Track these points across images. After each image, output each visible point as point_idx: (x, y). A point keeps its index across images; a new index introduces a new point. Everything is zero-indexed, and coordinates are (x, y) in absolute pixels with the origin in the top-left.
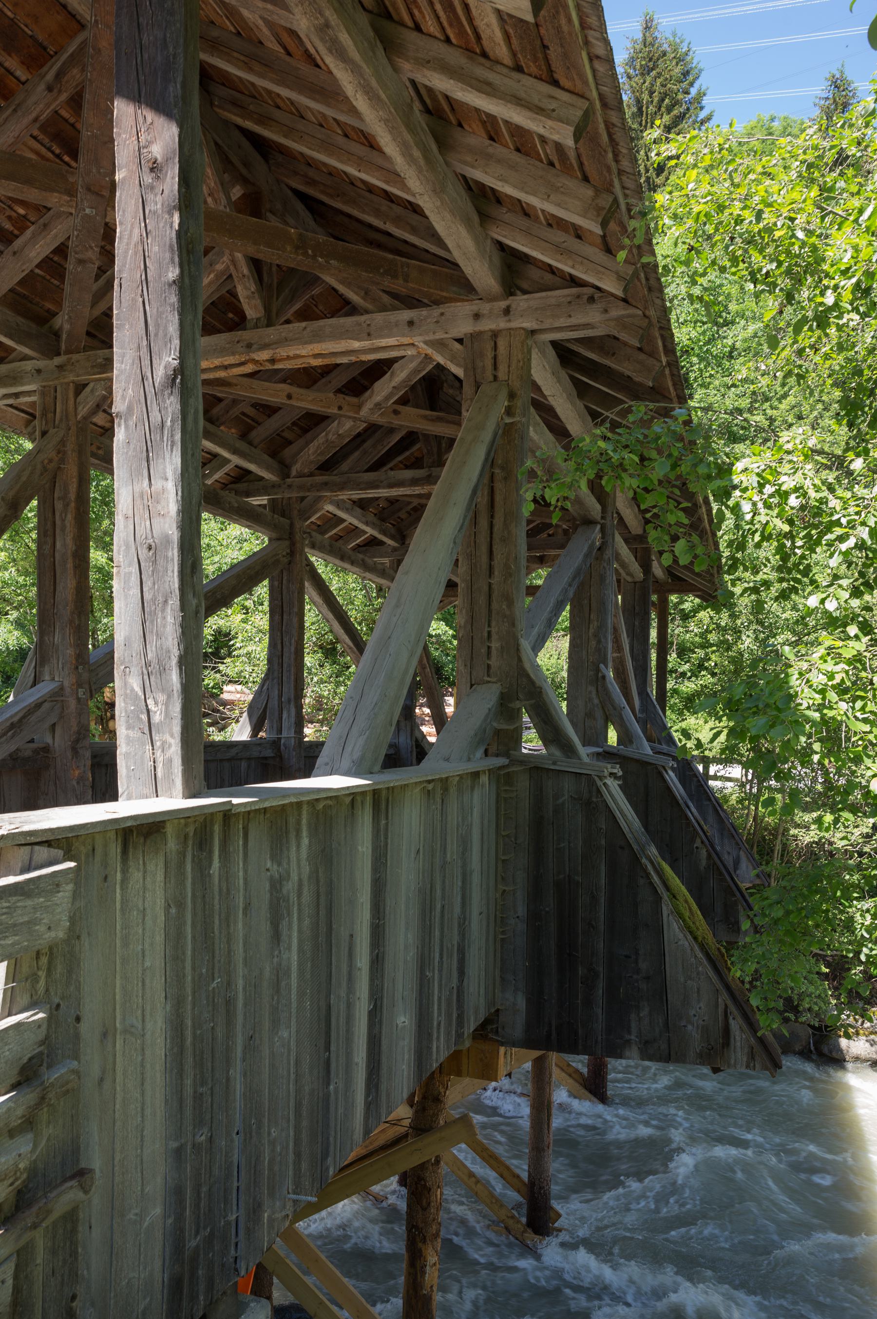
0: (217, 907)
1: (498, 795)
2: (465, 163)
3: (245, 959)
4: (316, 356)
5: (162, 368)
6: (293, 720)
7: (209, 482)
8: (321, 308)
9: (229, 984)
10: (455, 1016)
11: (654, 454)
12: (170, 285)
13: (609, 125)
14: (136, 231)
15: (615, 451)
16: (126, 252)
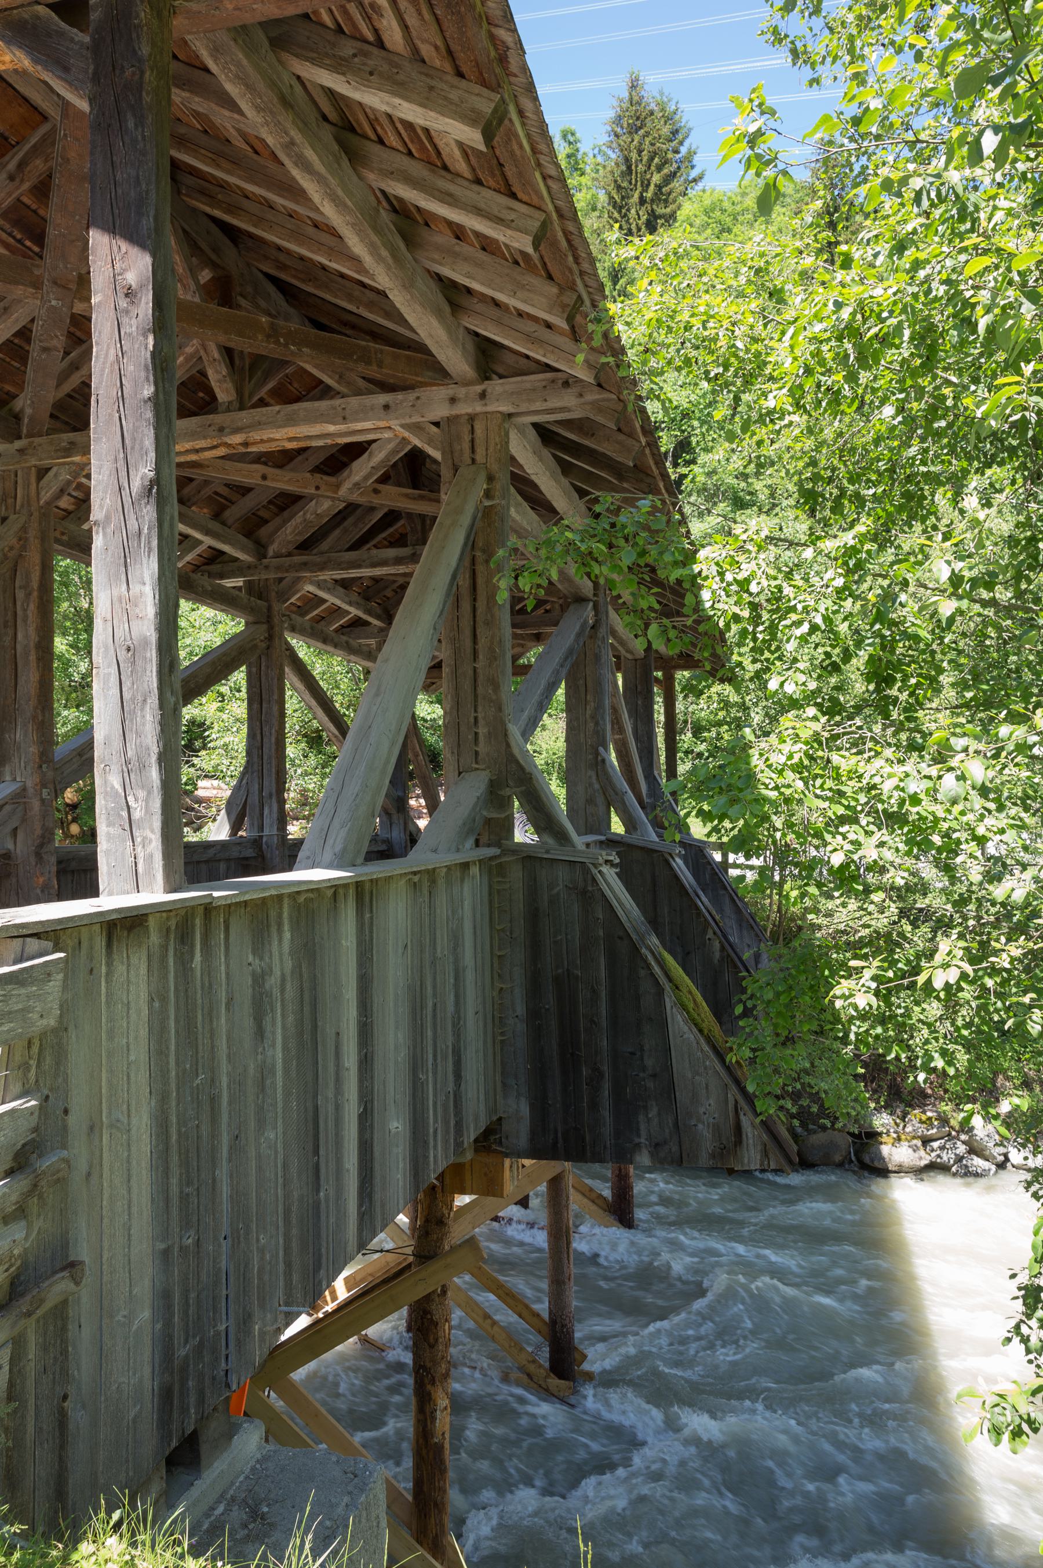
0: (199, 1001)
1: (490, 887)
2: (433, 260)
3: (229, 1056)
4: (290, 439)
5: (138, 478)
6: (275, 815)
7: (180, 565)
8: (296, 385)
9: (213, 1080)
10: (452, 1123)
11: (622, 542)
12: (145, 402)
13: (566, 234)
14: (112, 352)
15: (582, 541)
16: (103, 370)
